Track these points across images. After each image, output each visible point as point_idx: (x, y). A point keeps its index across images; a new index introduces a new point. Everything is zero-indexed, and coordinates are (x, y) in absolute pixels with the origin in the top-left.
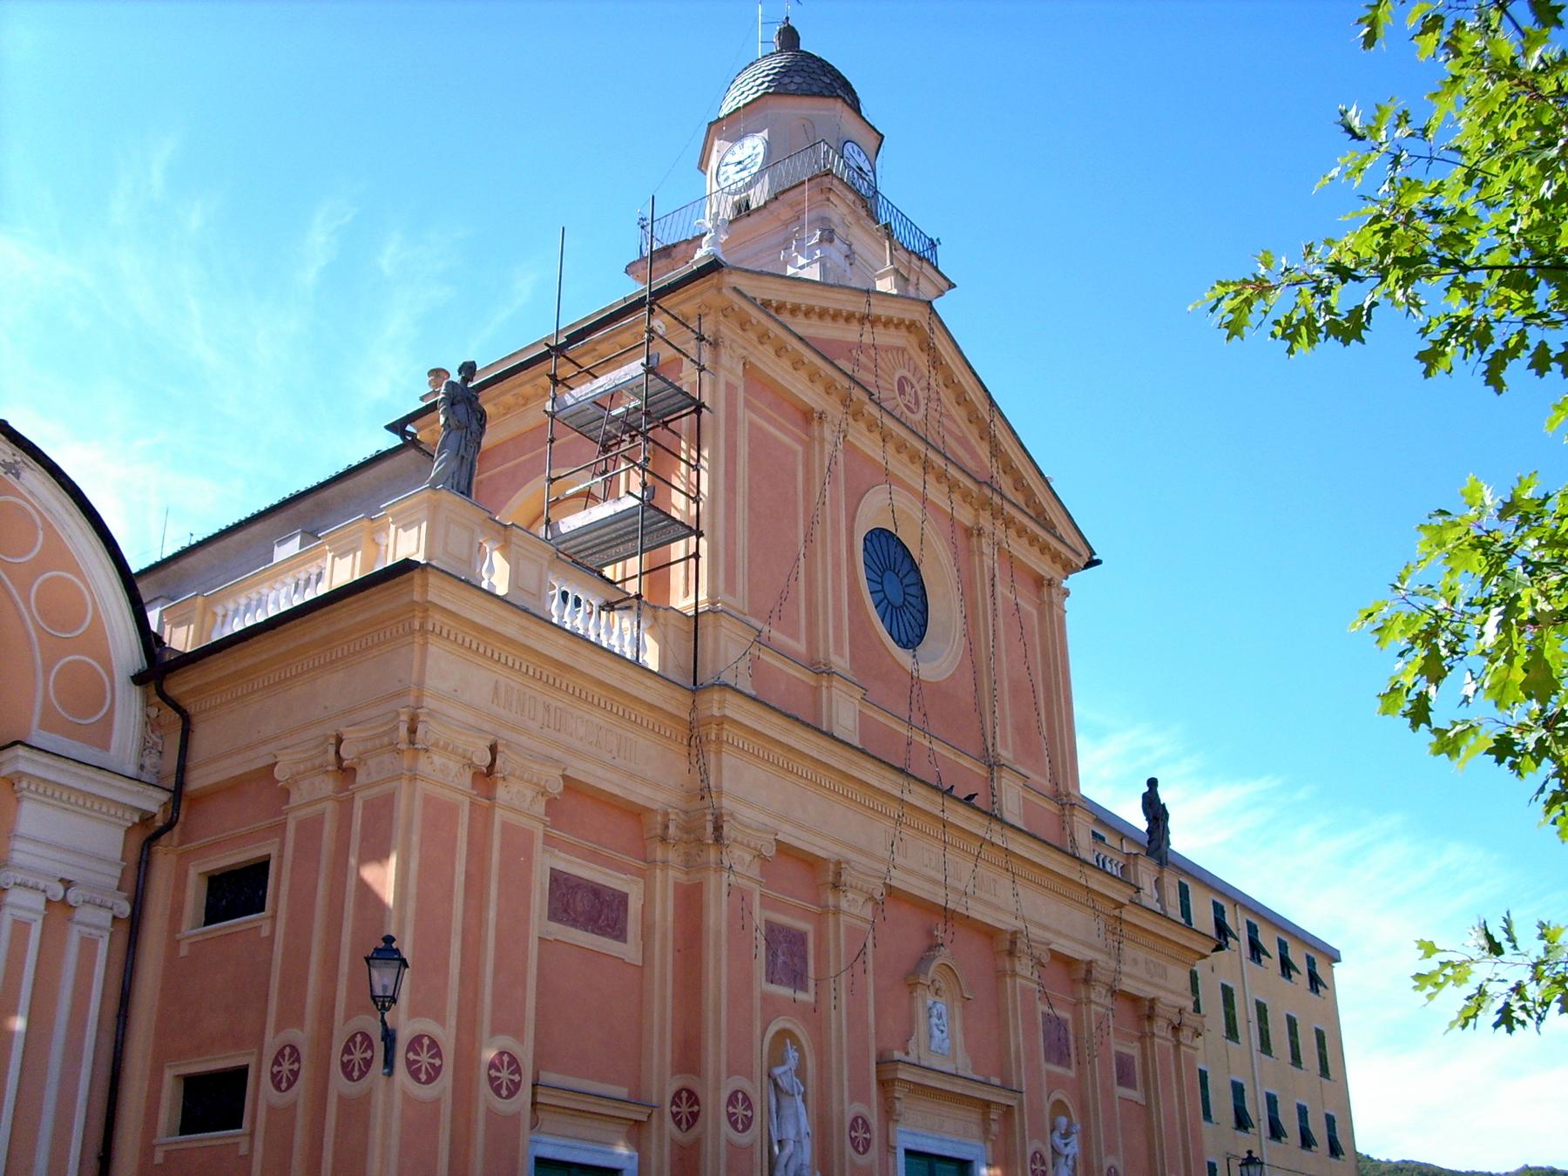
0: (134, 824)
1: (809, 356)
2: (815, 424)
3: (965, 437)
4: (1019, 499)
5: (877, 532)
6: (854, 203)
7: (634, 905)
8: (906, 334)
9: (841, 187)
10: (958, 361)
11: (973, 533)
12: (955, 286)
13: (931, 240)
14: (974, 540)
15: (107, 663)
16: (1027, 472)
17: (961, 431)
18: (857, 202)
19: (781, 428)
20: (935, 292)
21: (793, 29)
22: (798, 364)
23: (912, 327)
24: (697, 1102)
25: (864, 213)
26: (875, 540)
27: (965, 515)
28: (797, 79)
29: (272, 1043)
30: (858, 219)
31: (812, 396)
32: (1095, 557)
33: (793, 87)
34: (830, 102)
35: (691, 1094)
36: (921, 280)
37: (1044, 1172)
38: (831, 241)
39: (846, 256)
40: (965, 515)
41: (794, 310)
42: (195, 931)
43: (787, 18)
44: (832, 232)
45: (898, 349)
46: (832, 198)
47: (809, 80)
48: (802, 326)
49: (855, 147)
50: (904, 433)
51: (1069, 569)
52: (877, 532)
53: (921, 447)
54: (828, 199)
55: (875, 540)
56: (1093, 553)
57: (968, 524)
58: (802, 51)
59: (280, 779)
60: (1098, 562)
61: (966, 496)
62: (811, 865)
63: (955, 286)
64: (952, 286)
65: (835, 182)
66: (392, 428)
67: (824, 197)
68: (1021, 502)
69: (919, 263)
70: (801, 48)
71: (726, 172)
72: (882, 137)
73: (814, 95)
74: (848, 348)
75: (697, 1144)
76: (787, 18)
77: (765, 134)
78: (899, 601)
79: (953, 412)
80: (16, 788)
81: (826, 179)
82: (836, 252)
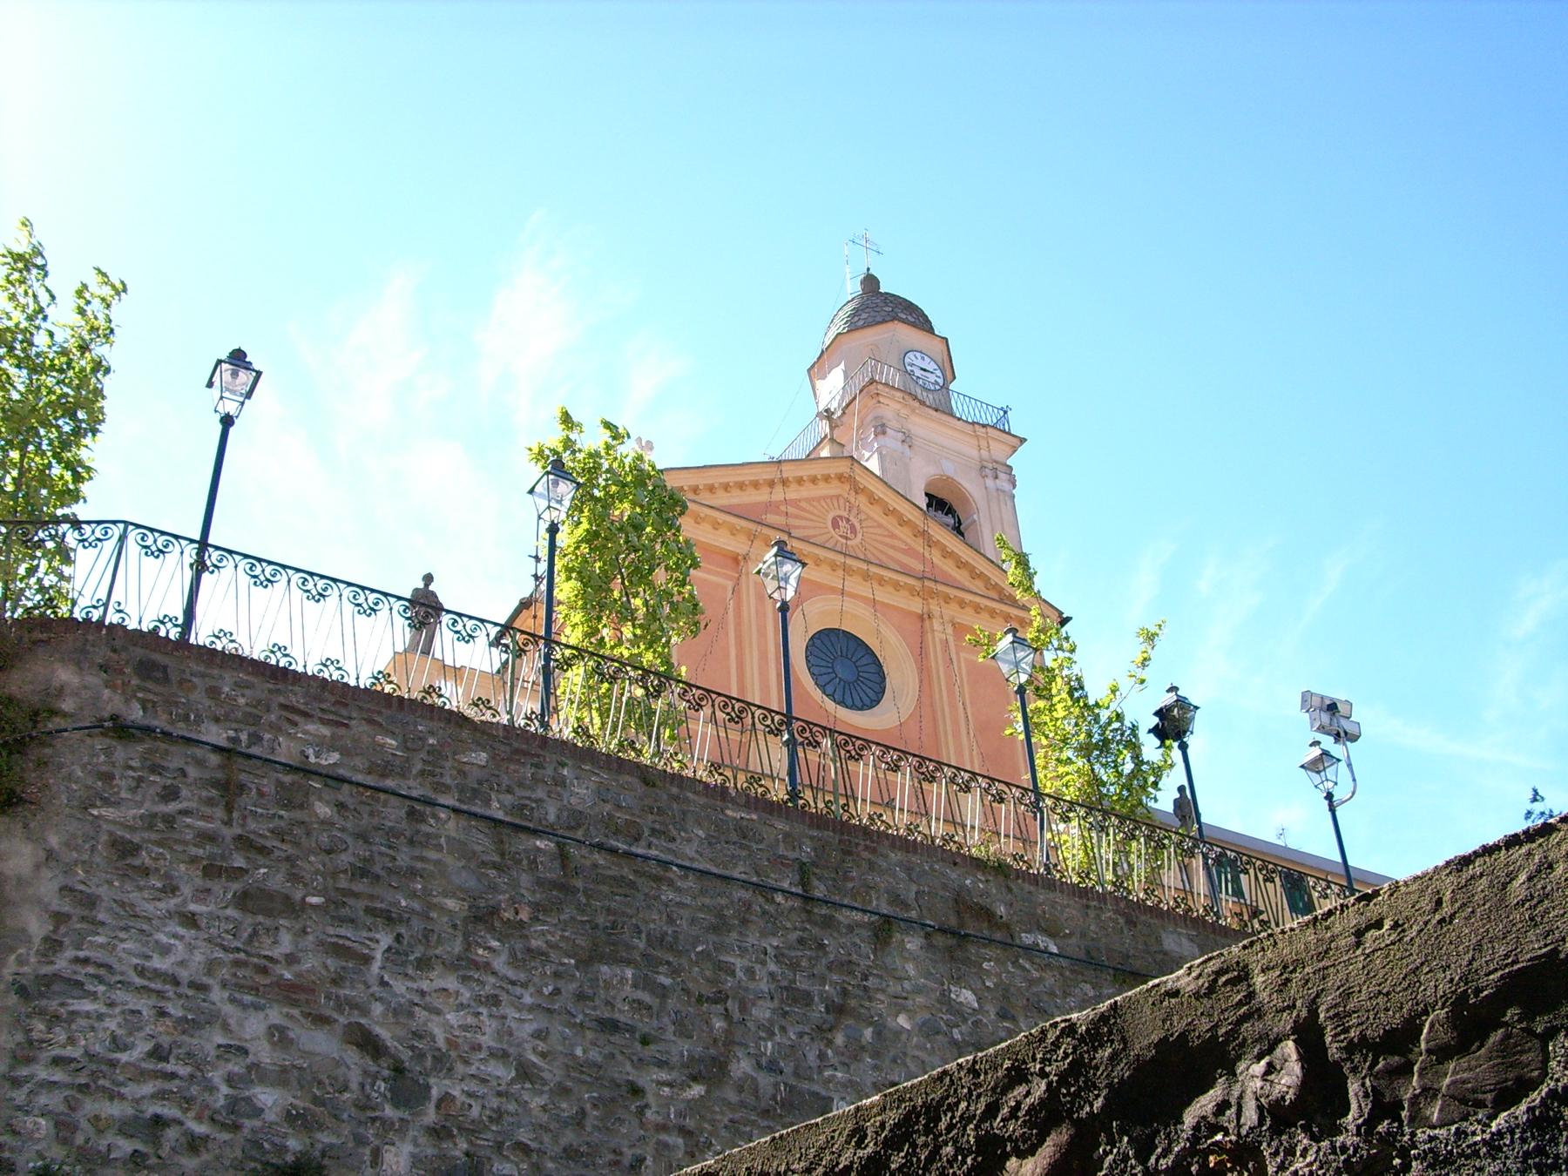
1: (721, 517)
3: (911, 548)
4: (978, 586)
6: (903, 398)
8: (840, 484)
9: (887, 390)
10: (890, 493)
11: (924, 618)
12: (1026, 440)
13: (1002, 409)
14: (927, 622)
16: (978, 563)
17: (906, 544)
18: (906, 397)
19: (717, 574)
20: (1008, 450)
21: (872, 275)
22: (716, 525)
23: (840, 477)
25: (917, 404)
27: (916, 606)
28: (864, 316)
30: (913, 410)
31: (738, 545)
32: (1064, 616)
33: (861, 323)
34: (890, 325)
36: (990, 442)
38: (884, 433)
39: (903, 441)
40: (916, 606)
41: (711, 489)
44: (883, 425)
45: (831, 497)
46: (881, 400)
47: (872, 314)
48: (722, 499)
49: (918, 355)
50: (831, 555)
53: (840, 559)
54: (879, 402)
56: (1061, 613)
57: (920, 612)
60: (1068, 619)
61: (912, 591)
62: (147, 669)
63: (1026, 440)
64: (1023, 441)
65: (880, 387)
67: (874, 401)
68: (982, 591)
69: (984, 430)
72: (946, 339)
73: (879, 323)
74: (770, 507)
76: (868, 269)
77: (842, 366)
78: (851, 678)
79: (897, 532)
81: (872, 387)
82: (892, 441)
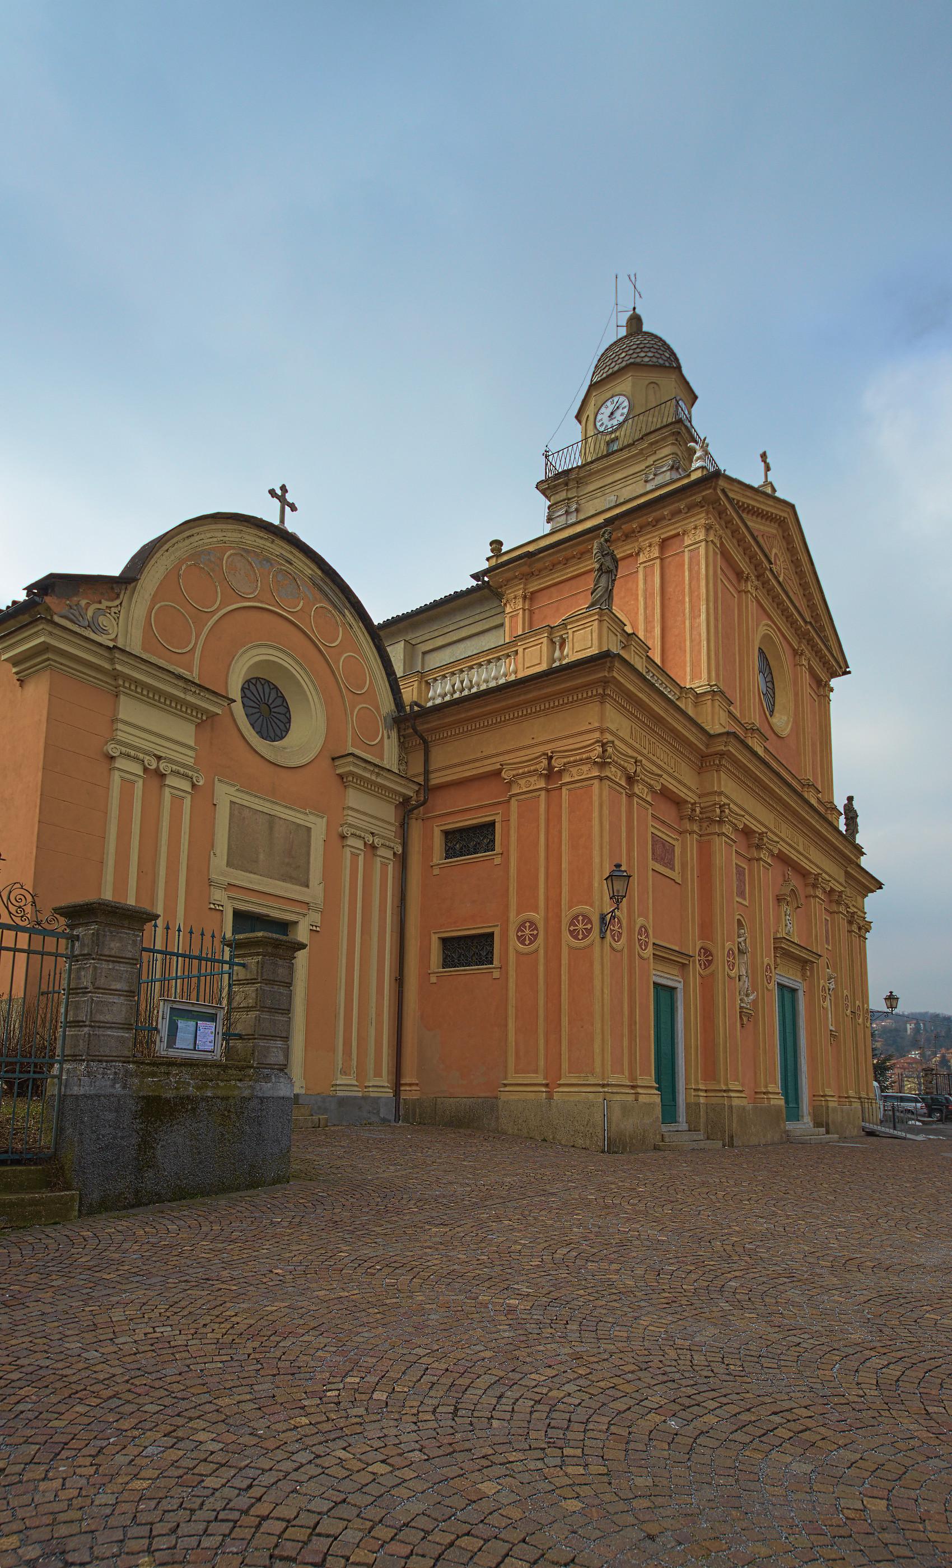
0: (400, 802)
2: (743, 582)
5: (254, 681)
7: (678, 851)
15: (378, 709)
24: (711, 955)
26: (252, 687)
29: (514, 919)
35: (706, 950)
37: (2, 1056)
42: (441, 862)
43: (634, 309)
51: (834, 675)
52: (254, 681)
55: (252, 687)
58: (646, 333)
59: (506, 777)
60: (849, 672)
66: (475, 577)
70: (645, 329)
71: (601, 420)
75: (712, 974)
76: (634, 309)
80: (345, 780)
81: (677, 426)
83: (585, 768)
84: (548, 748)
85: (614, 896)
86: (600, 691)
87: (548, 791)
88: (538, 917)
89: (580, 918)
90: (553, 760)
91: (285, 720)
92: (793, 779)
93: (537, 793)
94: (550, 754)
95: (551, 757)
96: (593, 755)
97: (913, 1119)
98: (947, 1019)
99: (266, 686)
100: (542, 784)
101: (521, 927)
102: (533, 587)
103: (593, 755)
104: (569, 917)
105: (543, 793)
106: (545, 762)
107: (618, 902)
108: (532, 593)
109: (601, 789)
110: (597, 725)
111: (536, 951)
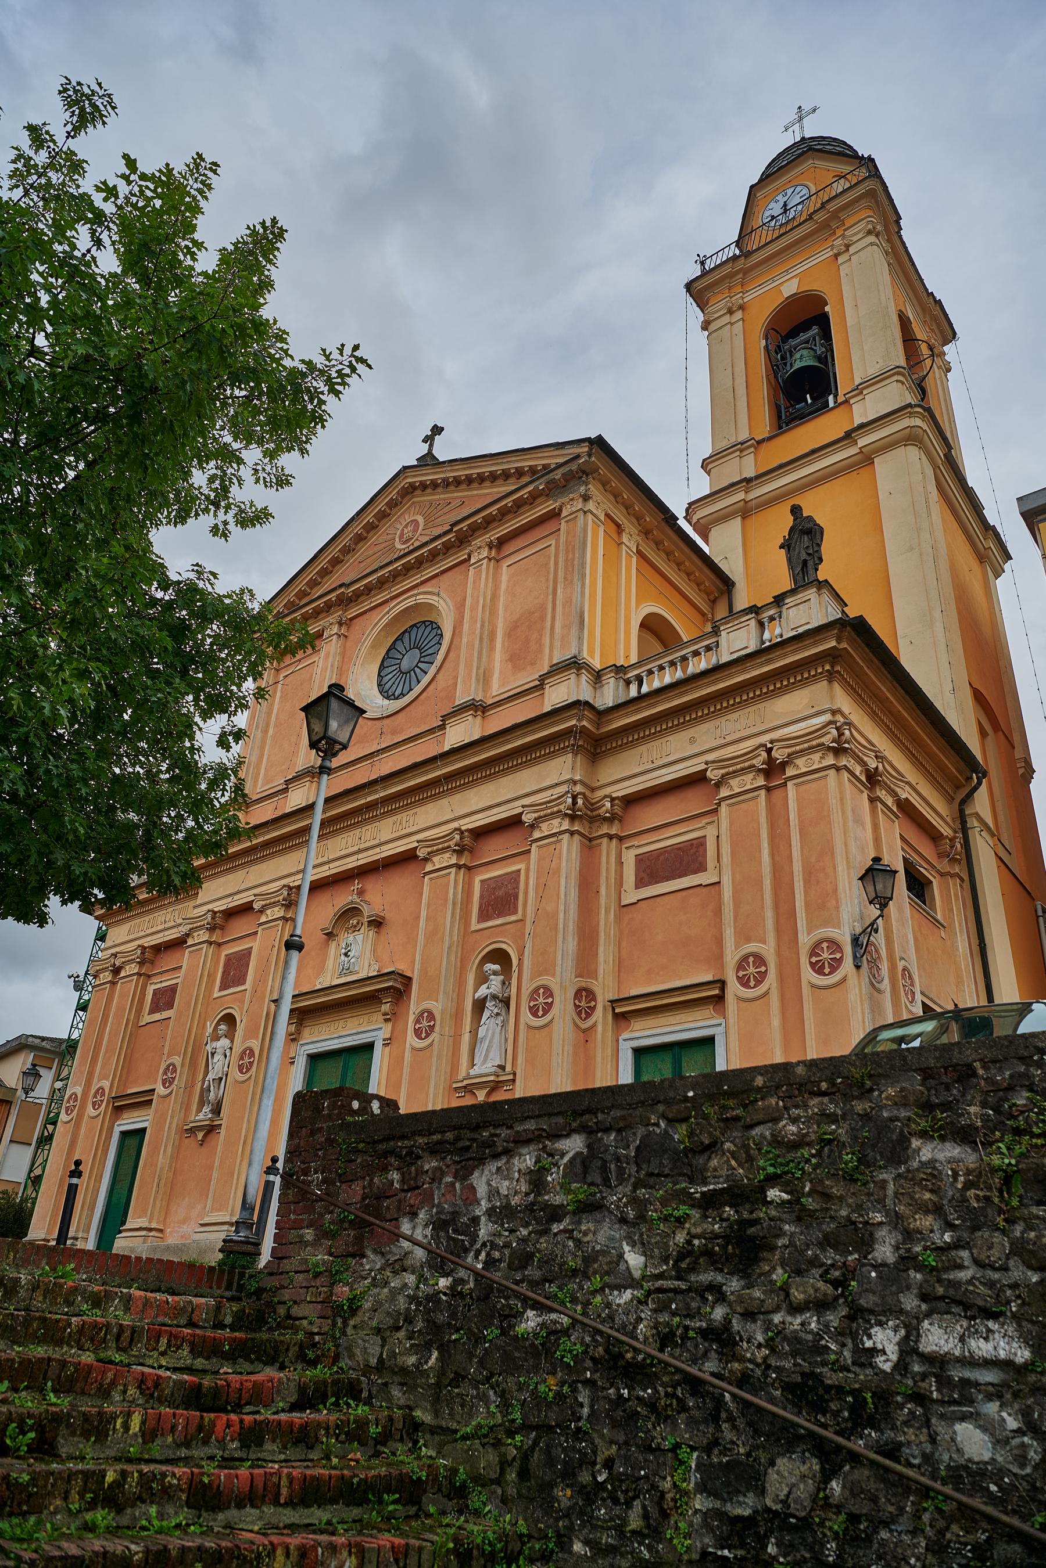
76: (360, 376)
83: (816, 757)
84: (765, 739)
85: (877, 897)
86: (827, 667)
87: (769, 790)
88: (768, 950)
89: (751, 959)
90: (773, 752)
91: (396, 694)
92: (108, 1016)
93: (756, 793)
94: (769, 746)
95: (771, 749)
96: (826, 740)
97: (557, 1311)
98: (1044, 1032)
99: (383, 683)
100: (761, 781)
101: (742, 964)
102: (352, 613)
103: (452, 843)
104: (737, 958)
105: (763, 792)
106: (764, 754)
107: (883, 906)
108: (351, 619)
109: (608, 846)
110: (568, 777)
111: (766, 994)
